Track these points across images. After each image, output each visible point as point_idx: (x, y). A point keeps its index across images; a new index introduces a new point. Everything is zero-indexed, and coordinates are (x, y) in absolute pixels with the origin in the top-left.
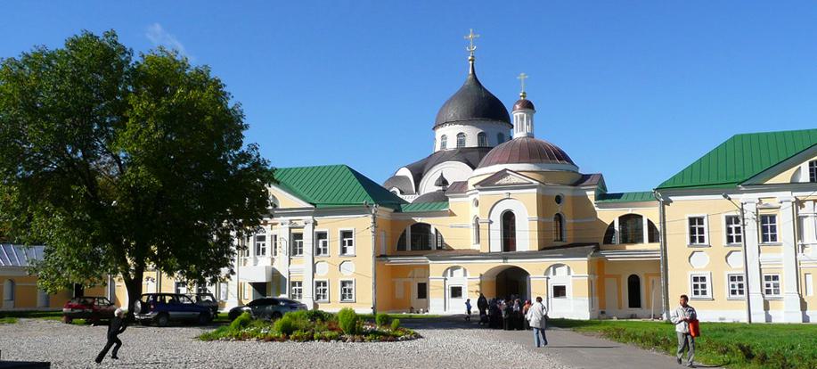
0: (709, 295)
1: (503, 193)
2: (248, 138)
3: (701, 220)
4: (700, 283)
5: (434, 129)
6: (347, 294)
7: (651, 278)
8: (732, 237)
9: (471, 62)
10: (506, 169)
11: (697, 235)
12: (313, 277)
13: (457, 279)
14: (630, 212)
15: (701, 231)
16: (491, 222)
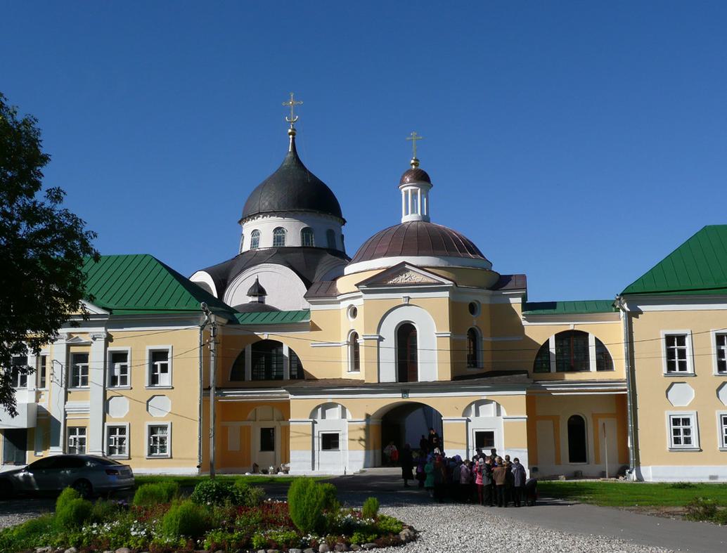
0: (694, 444)
1: (400, 297)
2: (49, 177)
3: (681, 339)
4: (681, 427)
5: (241, 222)
6: (158, 445)
7: (601, 421)
8: (161, 443)
9: (291, 137)
10: (404, 263)
11: (677, 360)
12: (104, 420)
13: (332, 422)
14: (571, 328)
15: (682, 354)
16: (381, 339)
